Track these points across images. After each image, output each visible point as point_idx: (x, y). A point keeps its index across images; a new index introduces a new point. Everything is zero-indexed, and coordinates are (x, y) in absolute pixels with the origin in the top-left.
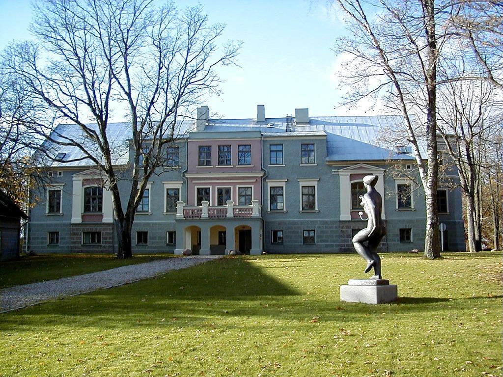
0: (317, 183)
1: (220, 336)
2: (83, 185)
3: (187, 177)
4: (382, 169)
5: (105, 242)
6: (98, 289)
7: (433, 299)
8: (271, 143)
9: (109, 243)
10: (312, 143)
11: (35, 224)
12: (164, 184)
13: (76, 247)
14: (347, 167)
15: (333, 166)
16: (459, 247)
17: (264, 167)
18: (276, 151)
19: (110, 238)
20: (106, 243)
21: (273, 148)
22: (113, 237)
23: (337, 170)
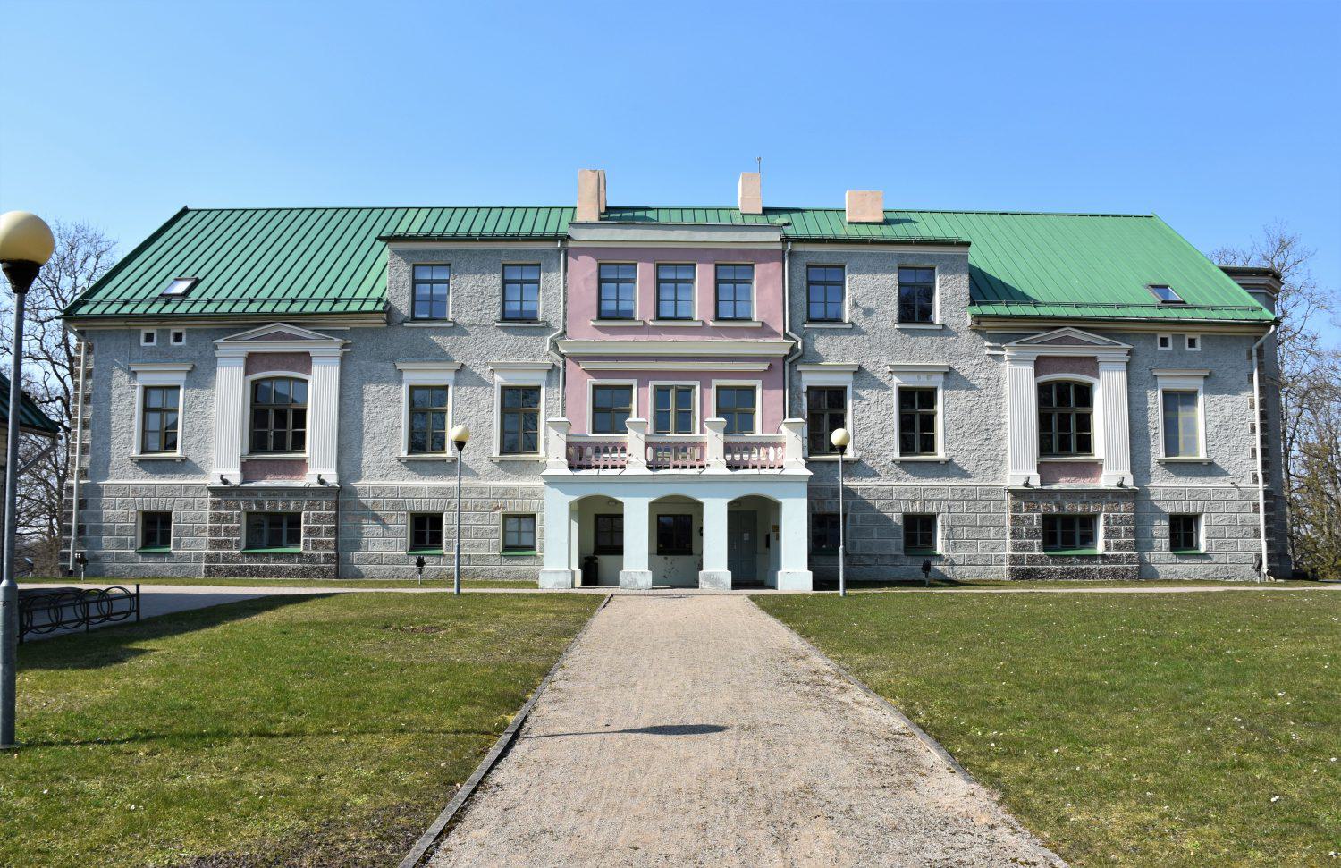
0: (1201, 382)
1: (1081, 750)
2: (247, 373)
3: (562, 351)
4: (1124, 345)
5: (314, 542)
6: (813, 639)
7: (655, 733)
8: (813, 260)
9: (326, 545)
10: (928, 264)
11: (118, 489)
12: (800, 372)
13: (226, 559)
14: (1026, 335)
15: (987, 332)
16: (768, 582)
17: (791, 330)
18: (825, 284)
19: (328, 531)
20: (316, 545)
21: (818, 276)
22: (336, 528)
23: (999, 345)
